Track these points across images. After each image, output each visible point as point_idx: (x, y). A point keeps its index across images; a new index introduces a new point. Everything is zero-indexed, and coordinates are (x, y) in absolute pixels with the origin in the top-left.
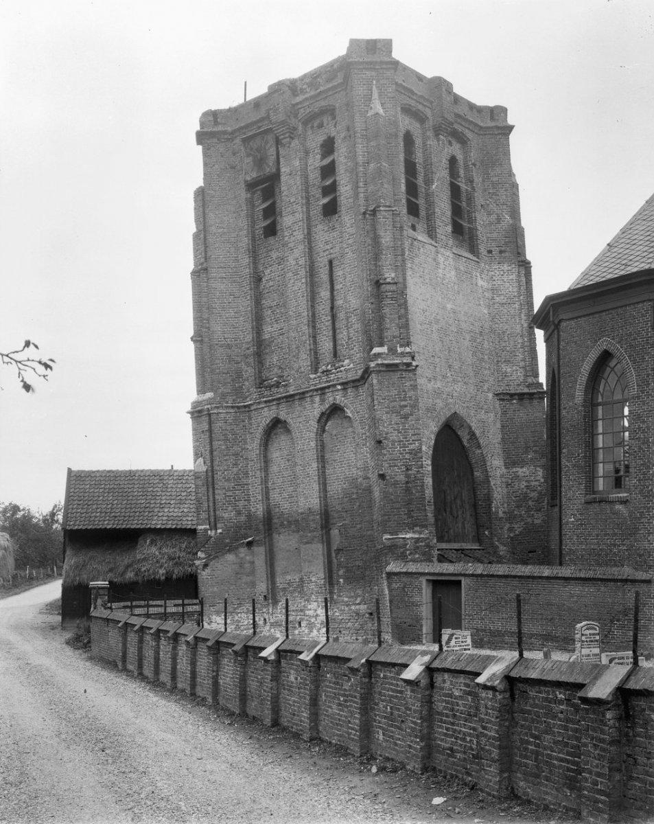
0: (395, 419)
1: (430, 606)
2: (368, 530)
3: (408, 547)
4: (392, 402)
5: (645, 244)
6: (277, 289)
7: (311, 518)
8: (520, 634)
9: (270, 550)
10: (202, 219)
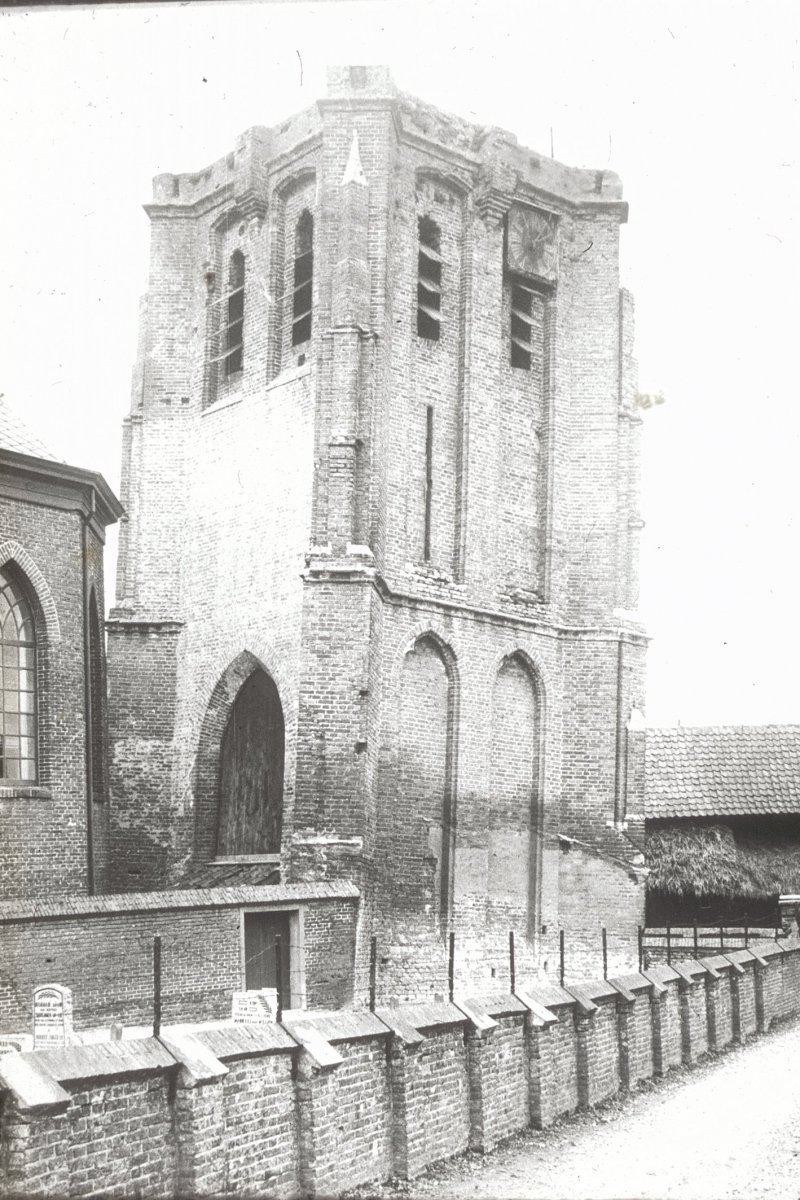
1: (294, 942)
8: (157, 1001)
10: (625, 304)
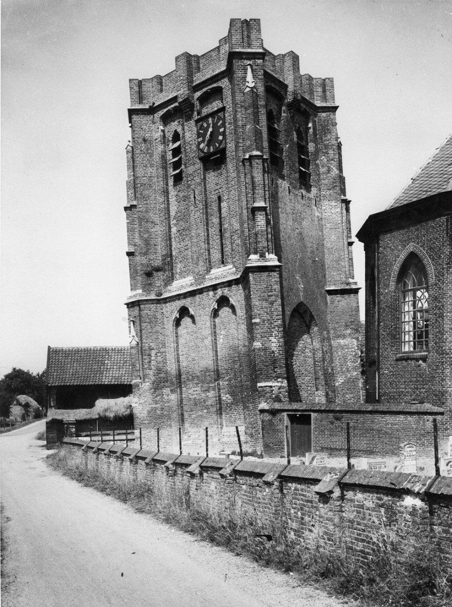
0: (265, 304)
2: (245, 382)
3: (274, 392)
4: (262, 293)
5: (440, 176)
6: (184, 218)
7: (208, 374)
8: (349, 450)
9: (374, 298)
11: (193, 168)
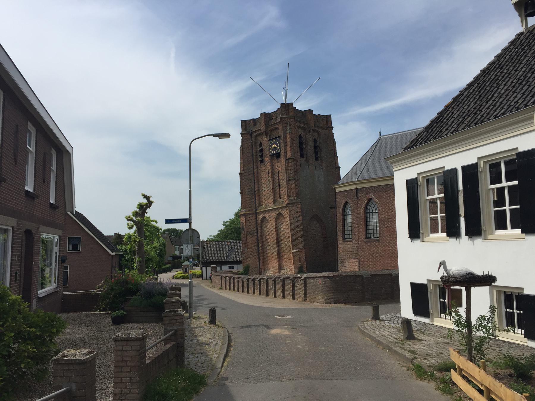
11: (267, 159)
